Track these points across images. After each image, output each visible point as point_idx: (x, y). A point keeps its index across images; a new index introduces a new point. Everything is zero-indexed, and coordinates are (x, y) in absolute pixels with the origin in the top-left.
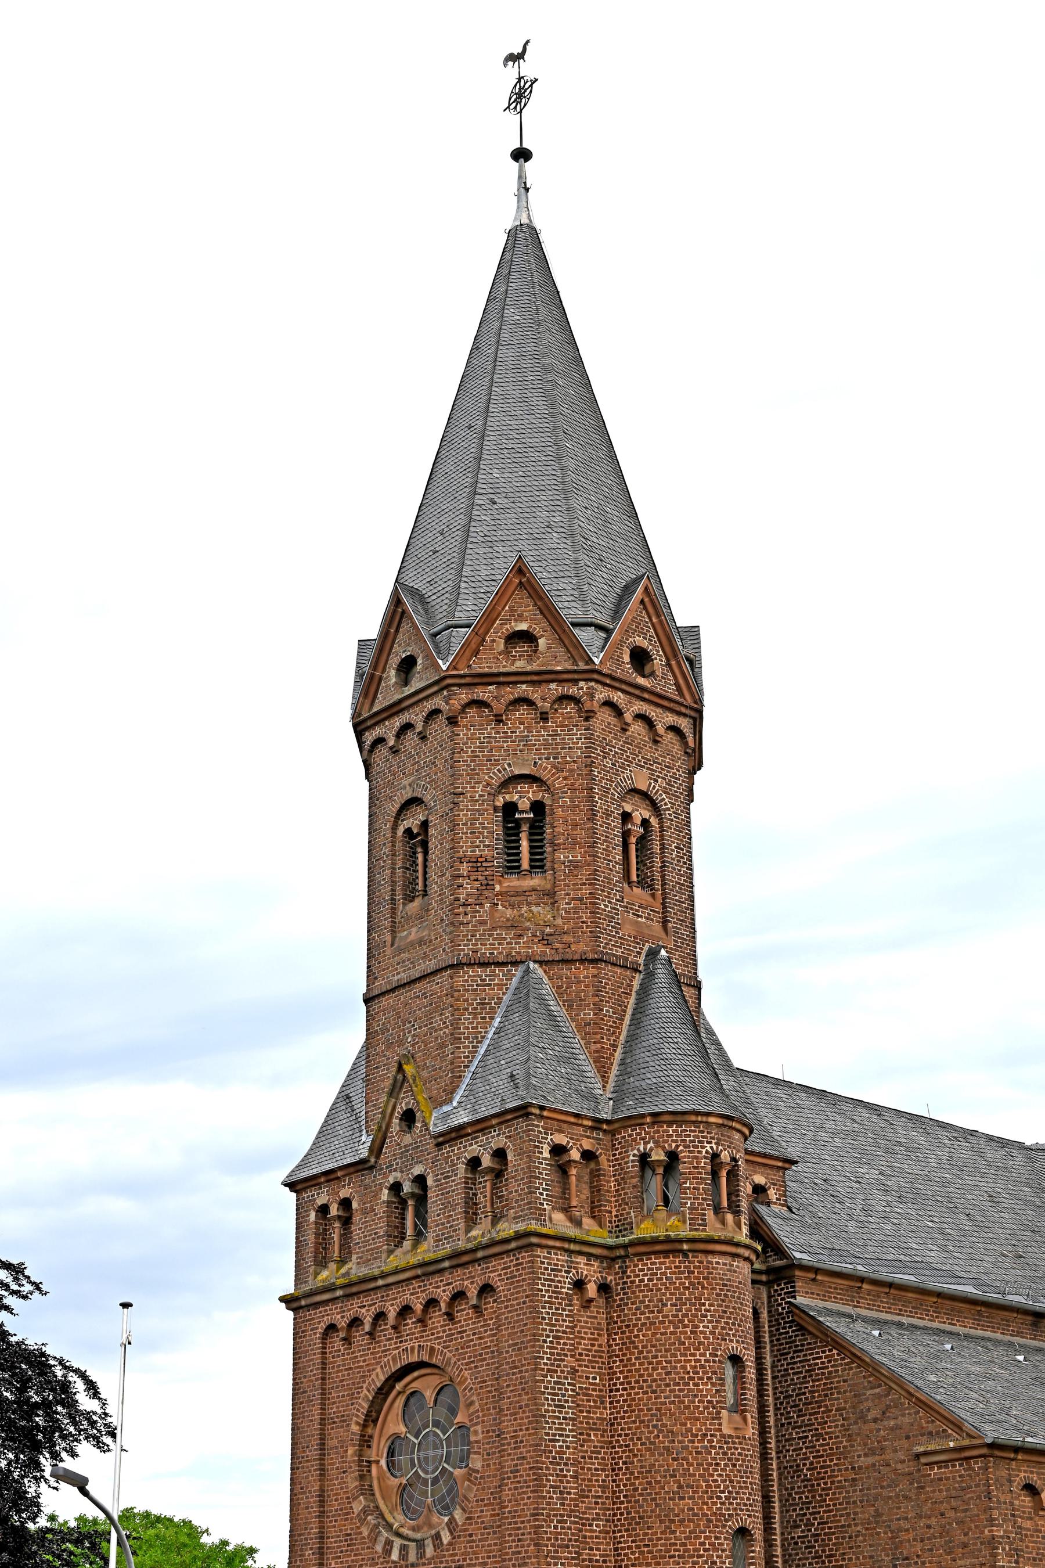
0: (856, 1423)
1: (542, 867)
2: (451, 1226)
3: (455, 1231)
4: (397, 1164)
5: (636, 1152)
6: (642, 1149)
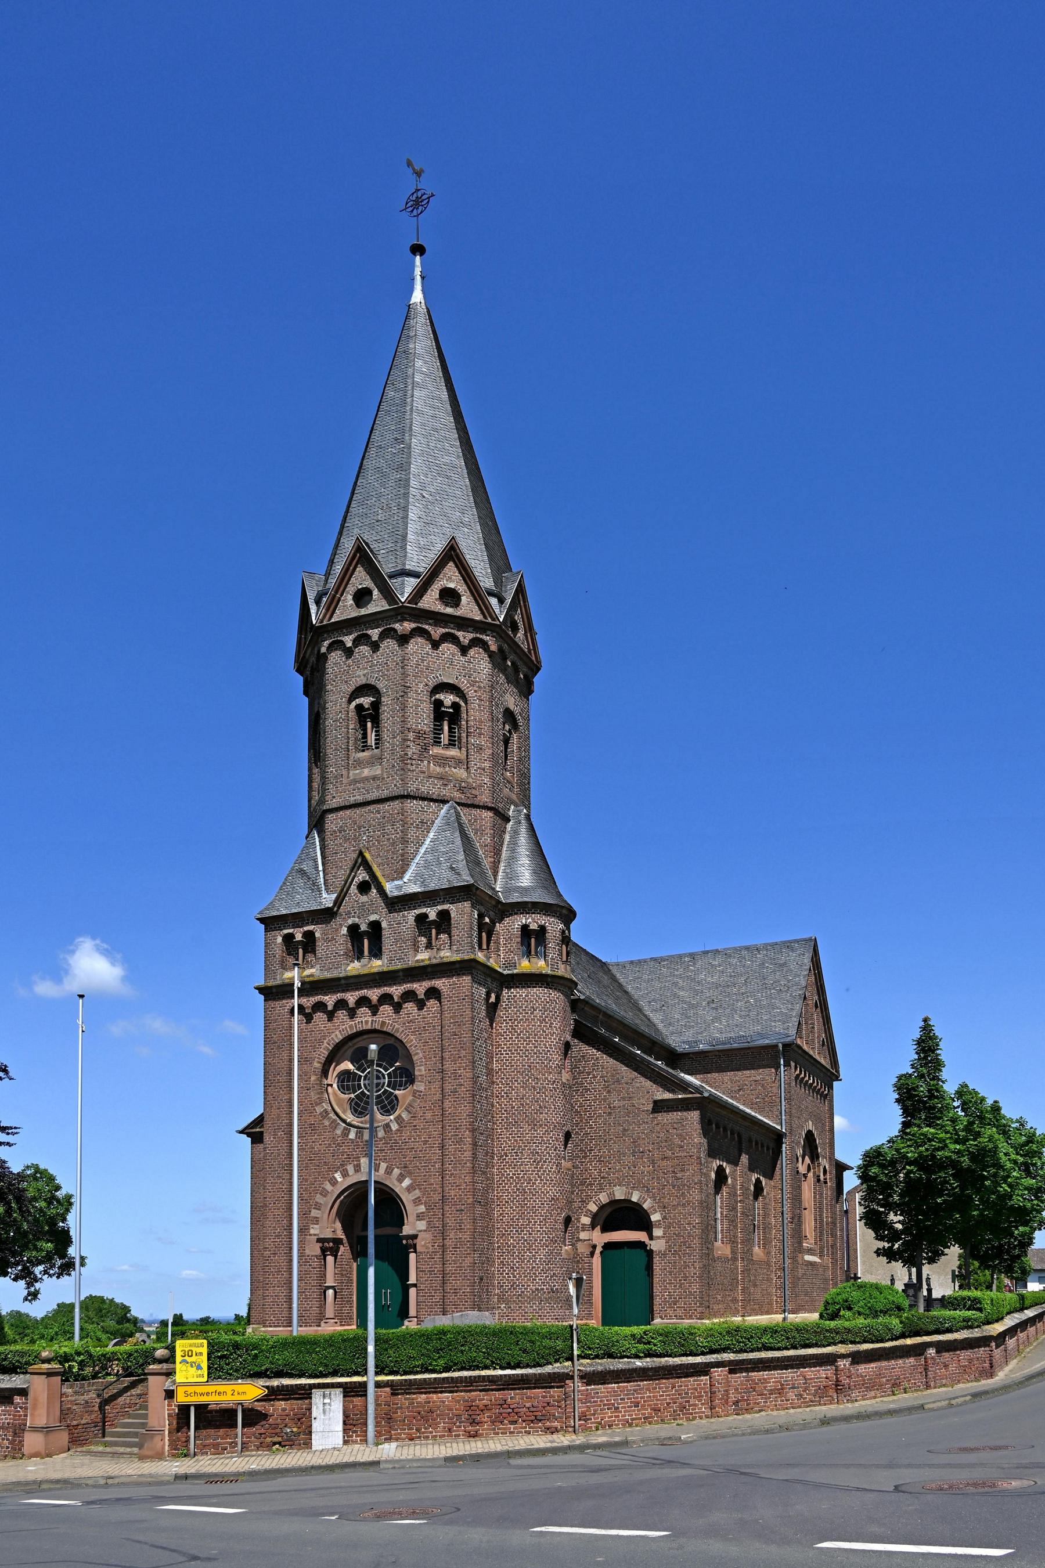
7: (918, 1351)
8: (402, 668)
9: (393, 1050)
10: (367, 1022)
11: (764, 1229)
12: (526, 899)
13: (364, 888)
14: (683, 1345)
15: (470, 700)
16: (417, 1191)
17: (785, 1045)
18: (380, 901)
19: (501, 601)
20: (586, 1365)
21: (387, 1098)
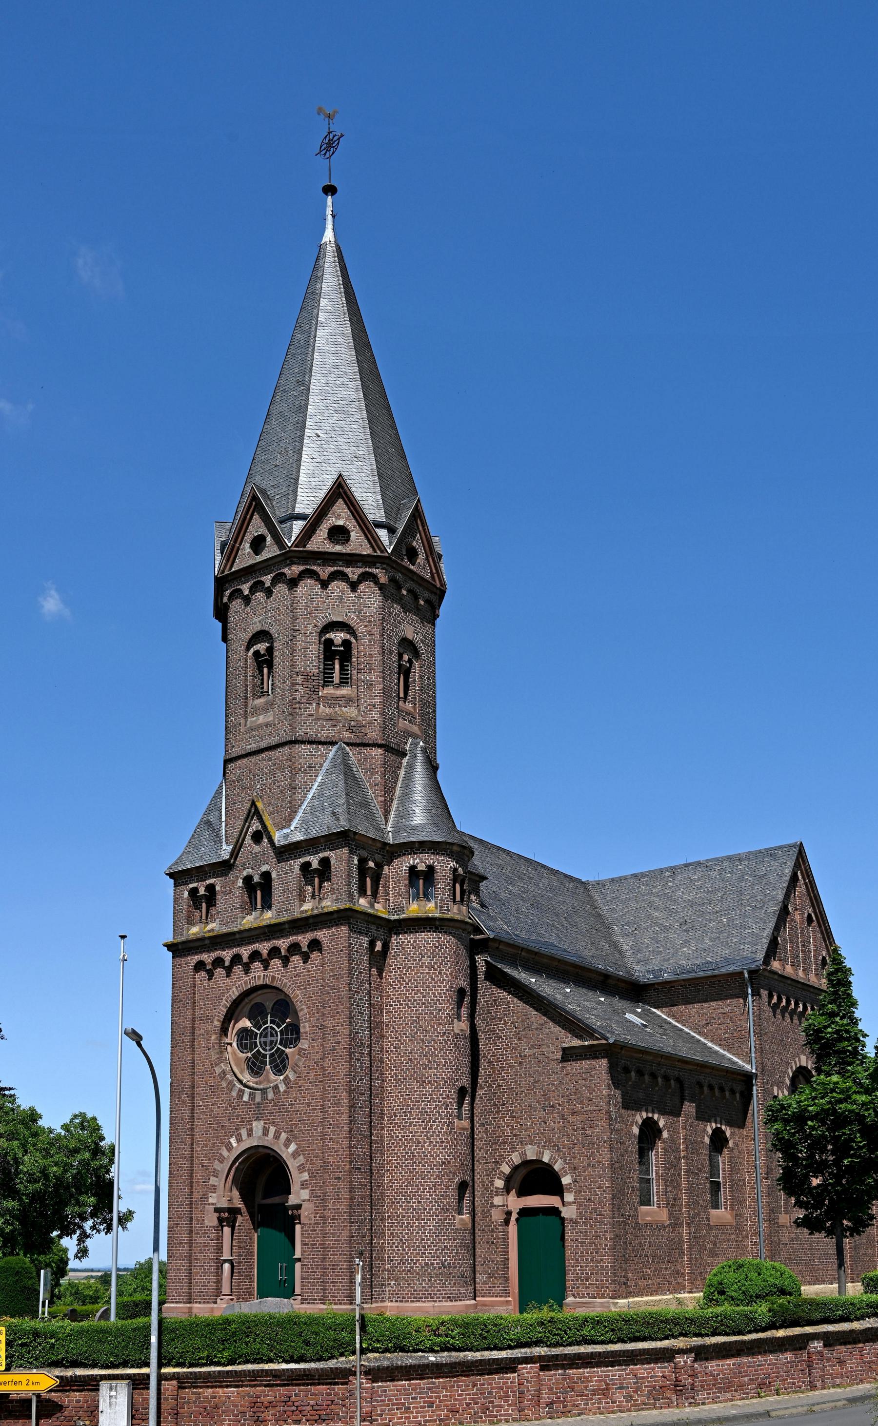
0: (524, 1030)
1: (347, 683)
7: (798, 1344)
9: (284, 1007)
10: (259, 977)
11: (731, 1186)
13: (257, 837)
14: (485, 1338)
16: (301, 1157)
17: (751, 972)
19: (392, 531)
20: (373, 1359)
21: (279, 1057)
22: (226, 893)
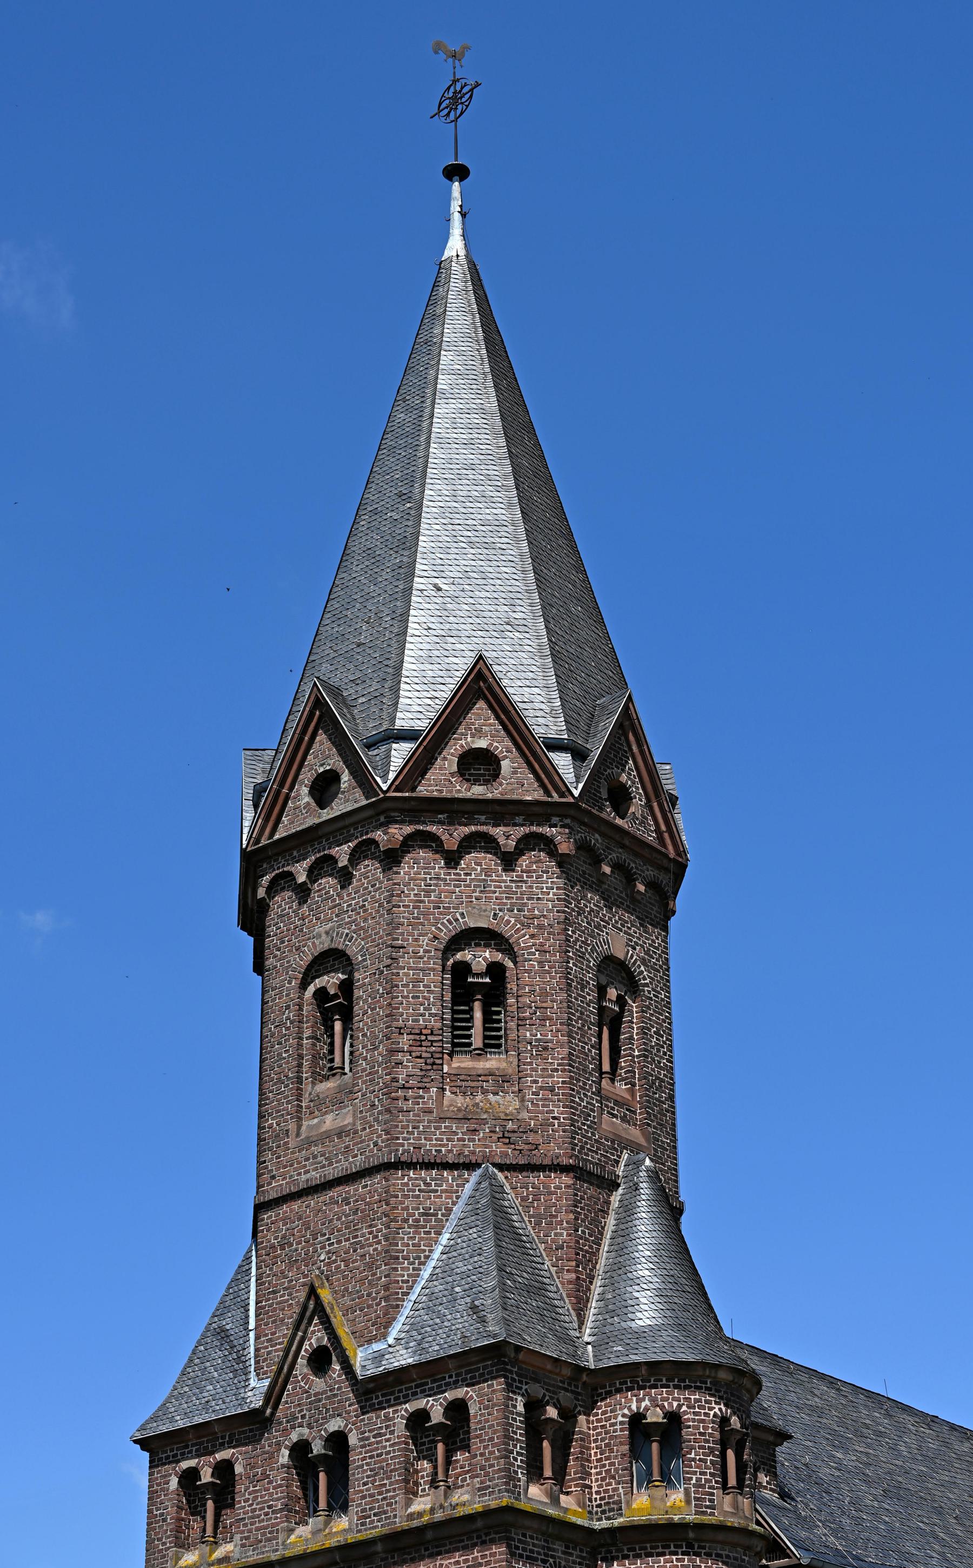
1: (499, 1046)
2: (384, 1499)
3: (390, 1504)
4: (303, 1417)
5: (626, 1411)
6: (634, 1407)
8: (389, 912)
12: (634, 1358)
13: (320, 1360)
15: (522, 953)
18: (346, 1389)
19: (579, 755)
22: (254, 1480)
